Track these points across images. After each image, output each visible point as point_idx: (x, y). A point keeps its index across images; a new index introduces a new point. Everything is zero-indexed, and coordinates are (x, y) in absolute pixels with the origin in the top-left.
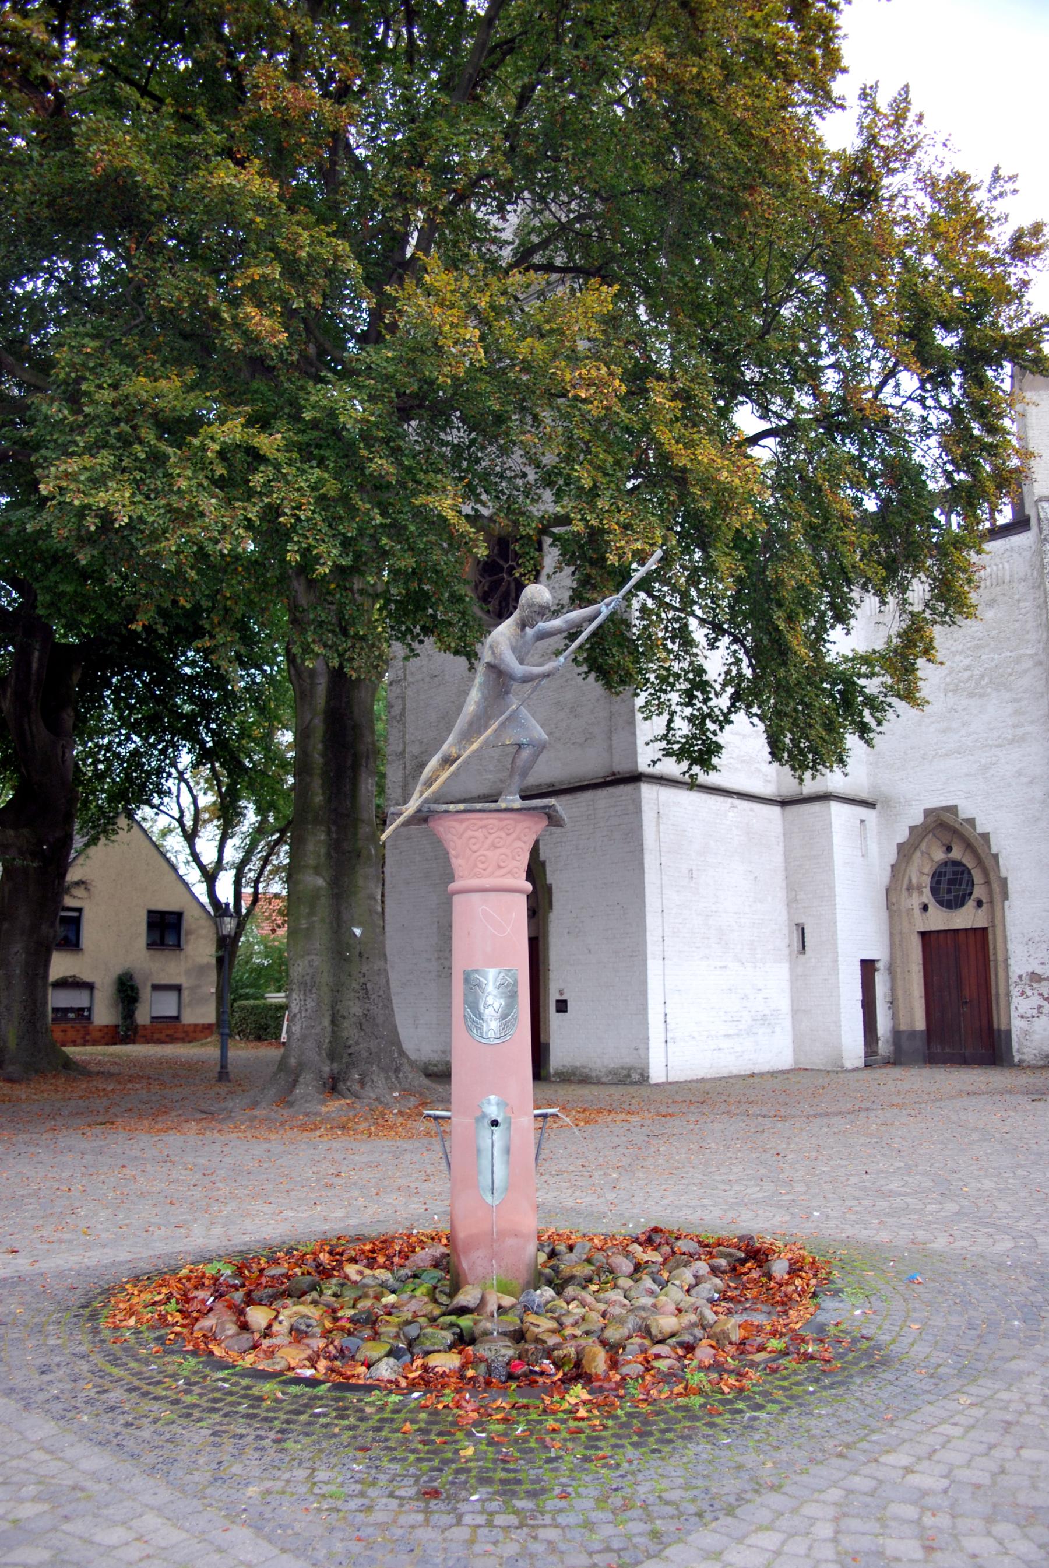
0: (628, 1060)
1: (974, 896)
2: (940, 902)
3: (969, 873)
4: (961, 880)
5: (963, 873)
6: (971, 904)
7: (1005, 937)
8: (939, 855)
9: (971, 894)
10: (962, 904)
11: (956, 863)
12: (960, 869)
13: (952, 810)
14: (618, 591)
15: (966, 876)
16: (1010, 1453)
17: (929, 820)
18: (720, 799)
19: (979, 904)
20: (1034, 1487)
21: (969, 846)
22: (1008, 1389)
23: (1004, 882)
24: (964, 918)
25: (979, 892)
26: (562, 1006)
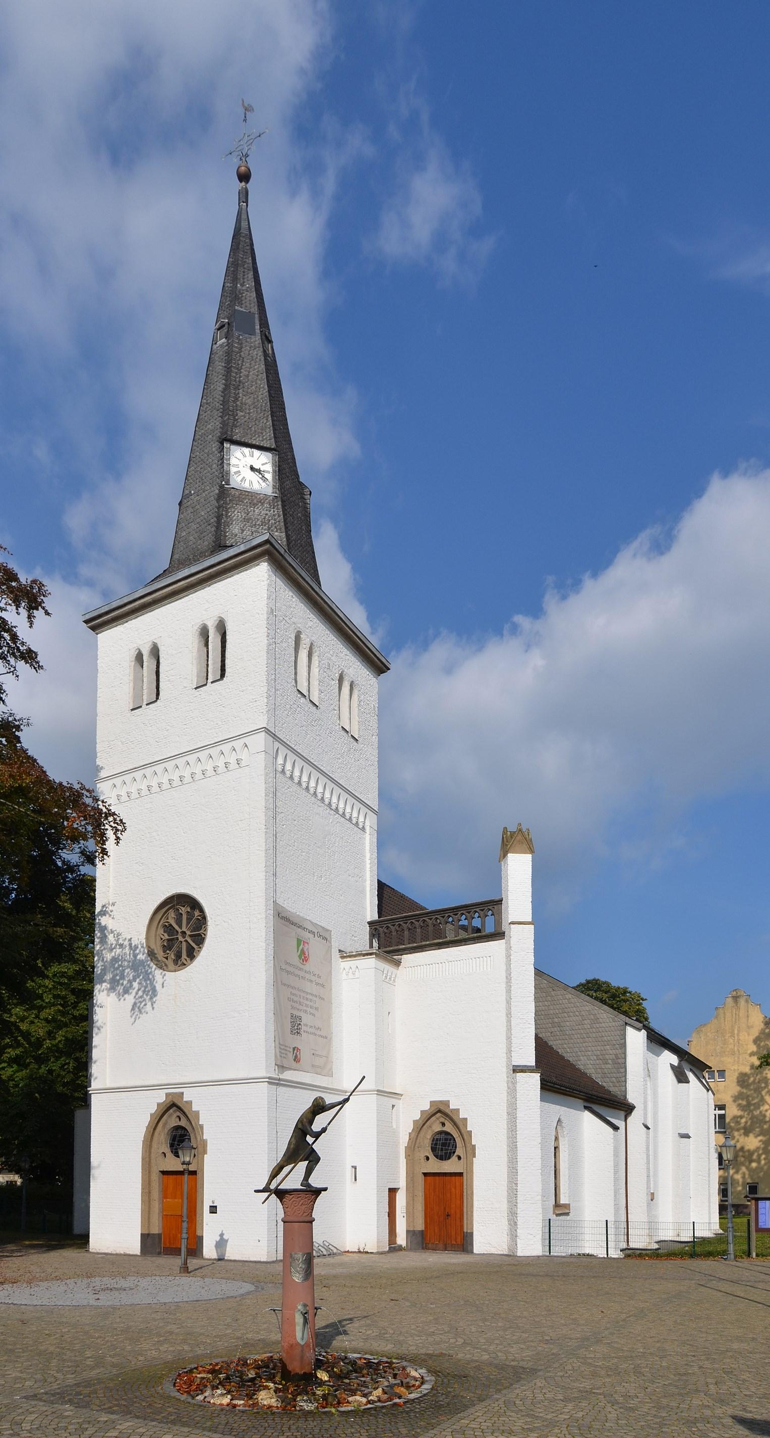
0: (191, 1176)
1: (456, 1154)
2: (436, 1156)
3: (455, 1140)
4: (449, 1143)
5: (450, 1140)
6: (454, 1158)
7: (232, 576)
8: (438, 1128)
9: (454, 1152)
10: (449, 1158)
11: (447, 1133)
12: (449, 1137)
13: (447, 1103)
14: (191, 932)
15: (452, 1141)
16: (496, 1419)
17: (433, 1109)
18: (291, 1089)
19: (459, 1158)
20: (503, 1426)
21: (455, 1124)
22: (494, 1403)
23: (474, 1147)
24: (449, 1166)
25: (459, 1151)
26: (213, 1210)
